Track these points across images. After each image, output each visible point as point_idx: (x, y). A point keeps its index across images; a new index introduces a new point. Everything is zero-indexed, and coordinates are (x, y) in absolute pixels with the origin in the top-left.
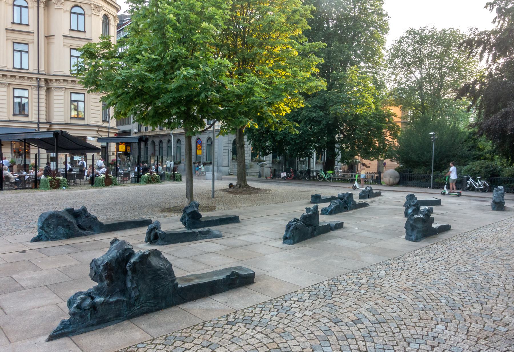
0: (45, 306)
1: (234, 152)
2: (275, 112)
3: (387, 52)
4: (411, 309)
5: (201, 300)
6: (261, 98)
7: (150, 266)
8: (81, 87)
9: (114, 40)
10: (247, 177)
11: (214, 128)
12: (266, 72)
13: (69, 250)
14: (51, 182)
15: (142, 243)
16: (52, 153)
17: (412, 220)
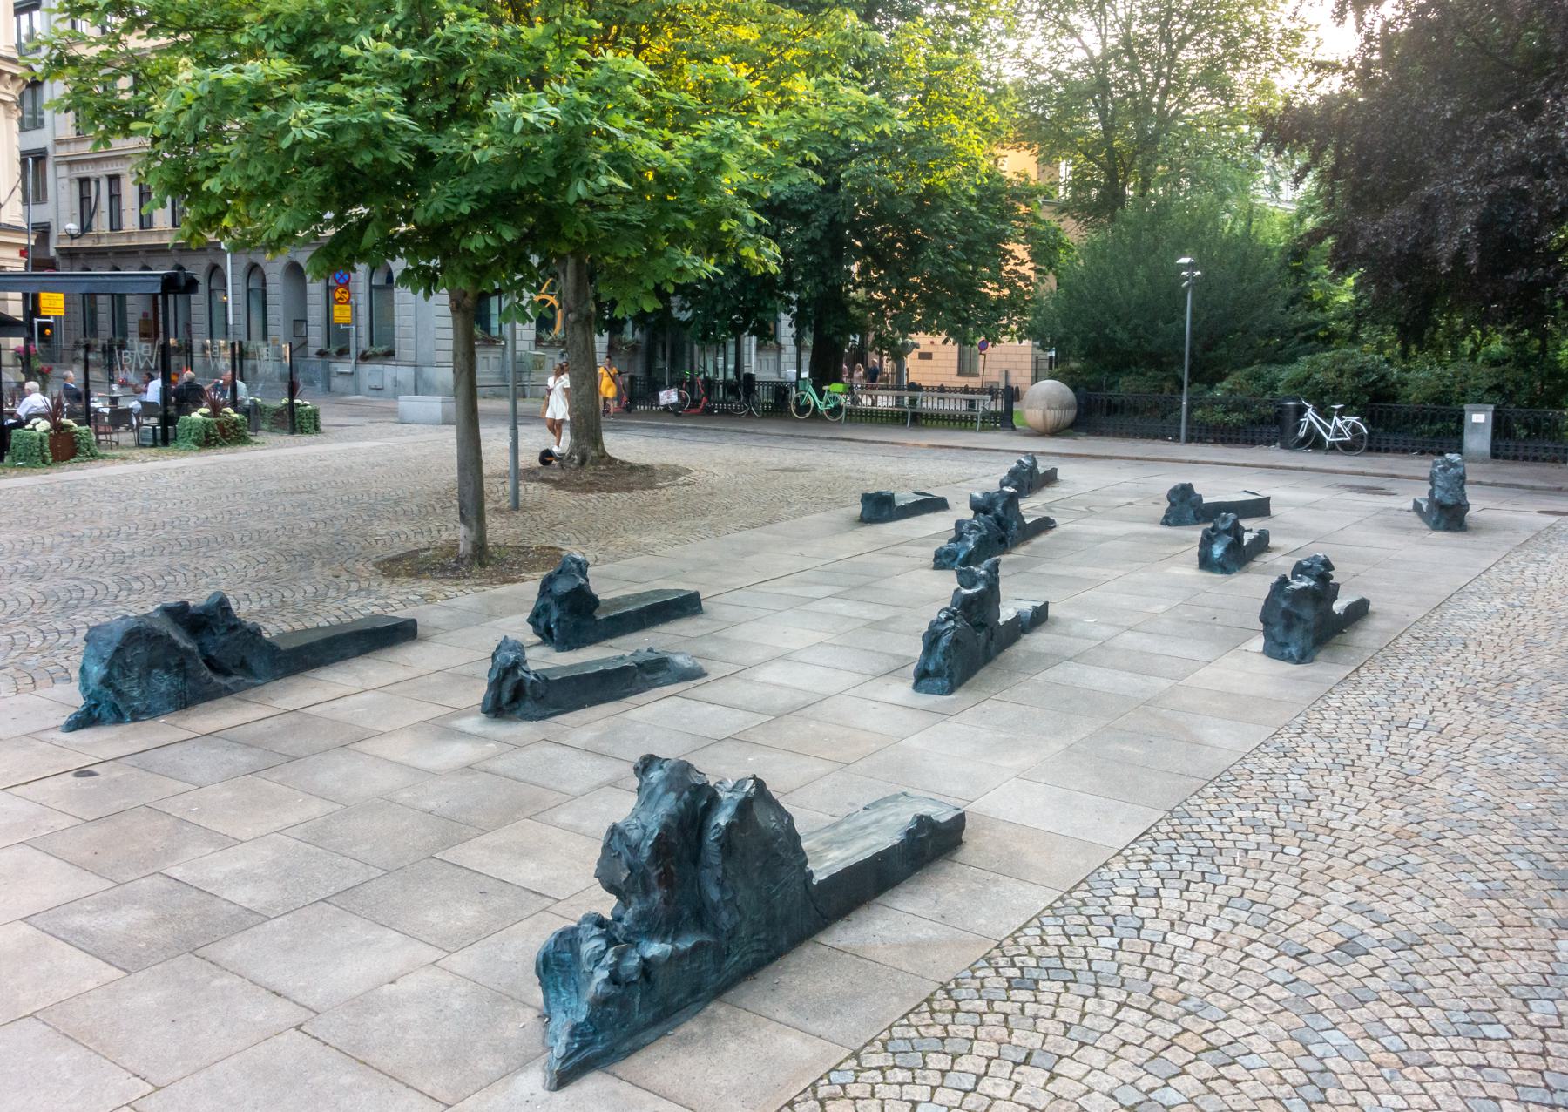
17: (1285, 597)
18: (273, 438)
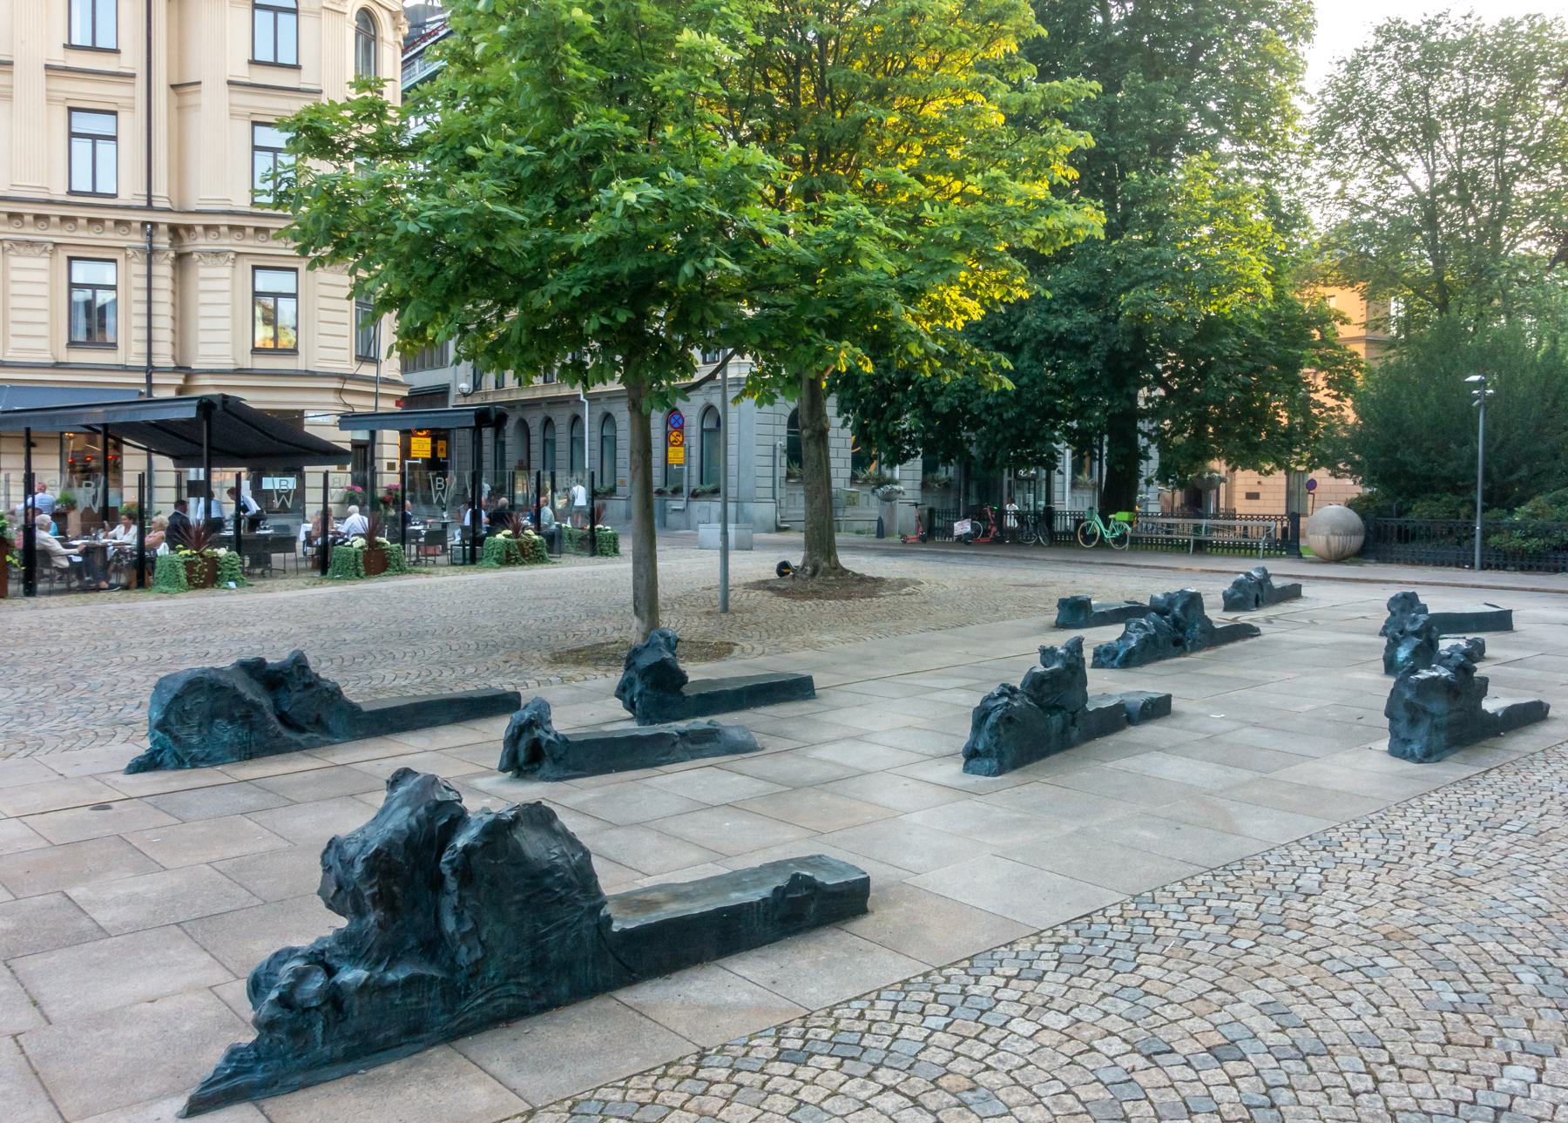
0: (174, 993)
1: (794, 452)
2: (930, 318)
3: (1311, 100)
4: (1414, 1007)
5: (688, 973)
6: (883, 276)
7: (518, 858)
8: (287, 248)
9: (391, 94)
10: (839, 538)
11: (725, 375)
12: (896, 184)
13: (251, 801)
14: (189, 565)
15: (489, 772)
16: (192, 470)
17: (1410, 687)
18: (574, 559)
